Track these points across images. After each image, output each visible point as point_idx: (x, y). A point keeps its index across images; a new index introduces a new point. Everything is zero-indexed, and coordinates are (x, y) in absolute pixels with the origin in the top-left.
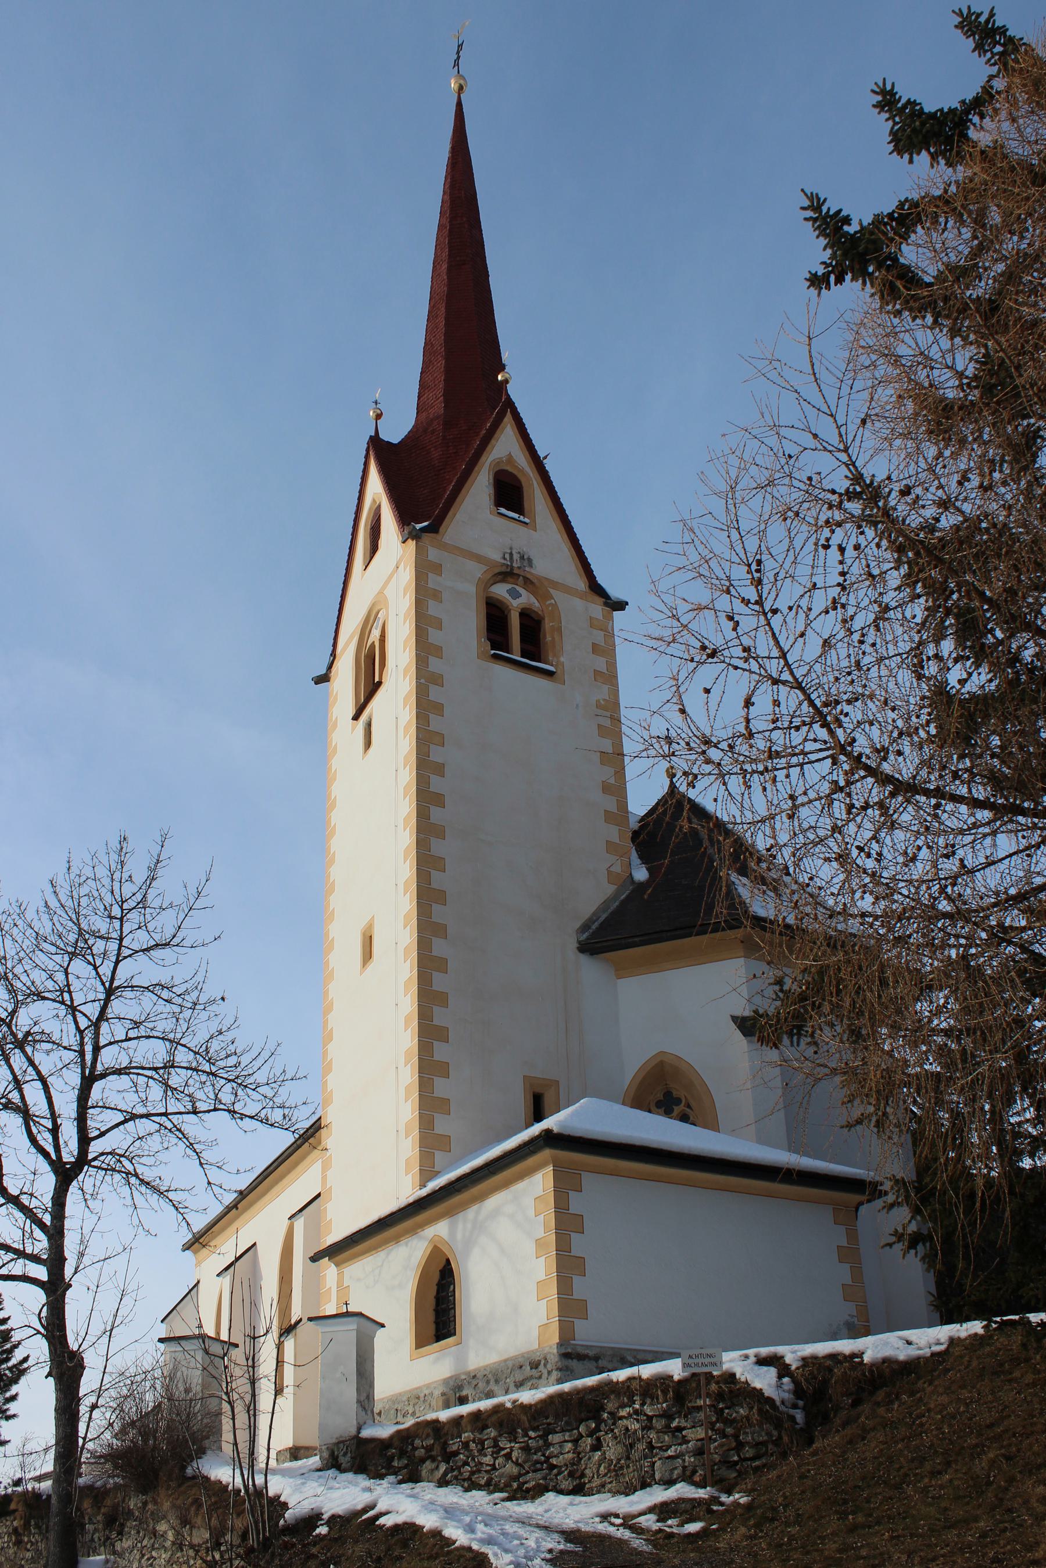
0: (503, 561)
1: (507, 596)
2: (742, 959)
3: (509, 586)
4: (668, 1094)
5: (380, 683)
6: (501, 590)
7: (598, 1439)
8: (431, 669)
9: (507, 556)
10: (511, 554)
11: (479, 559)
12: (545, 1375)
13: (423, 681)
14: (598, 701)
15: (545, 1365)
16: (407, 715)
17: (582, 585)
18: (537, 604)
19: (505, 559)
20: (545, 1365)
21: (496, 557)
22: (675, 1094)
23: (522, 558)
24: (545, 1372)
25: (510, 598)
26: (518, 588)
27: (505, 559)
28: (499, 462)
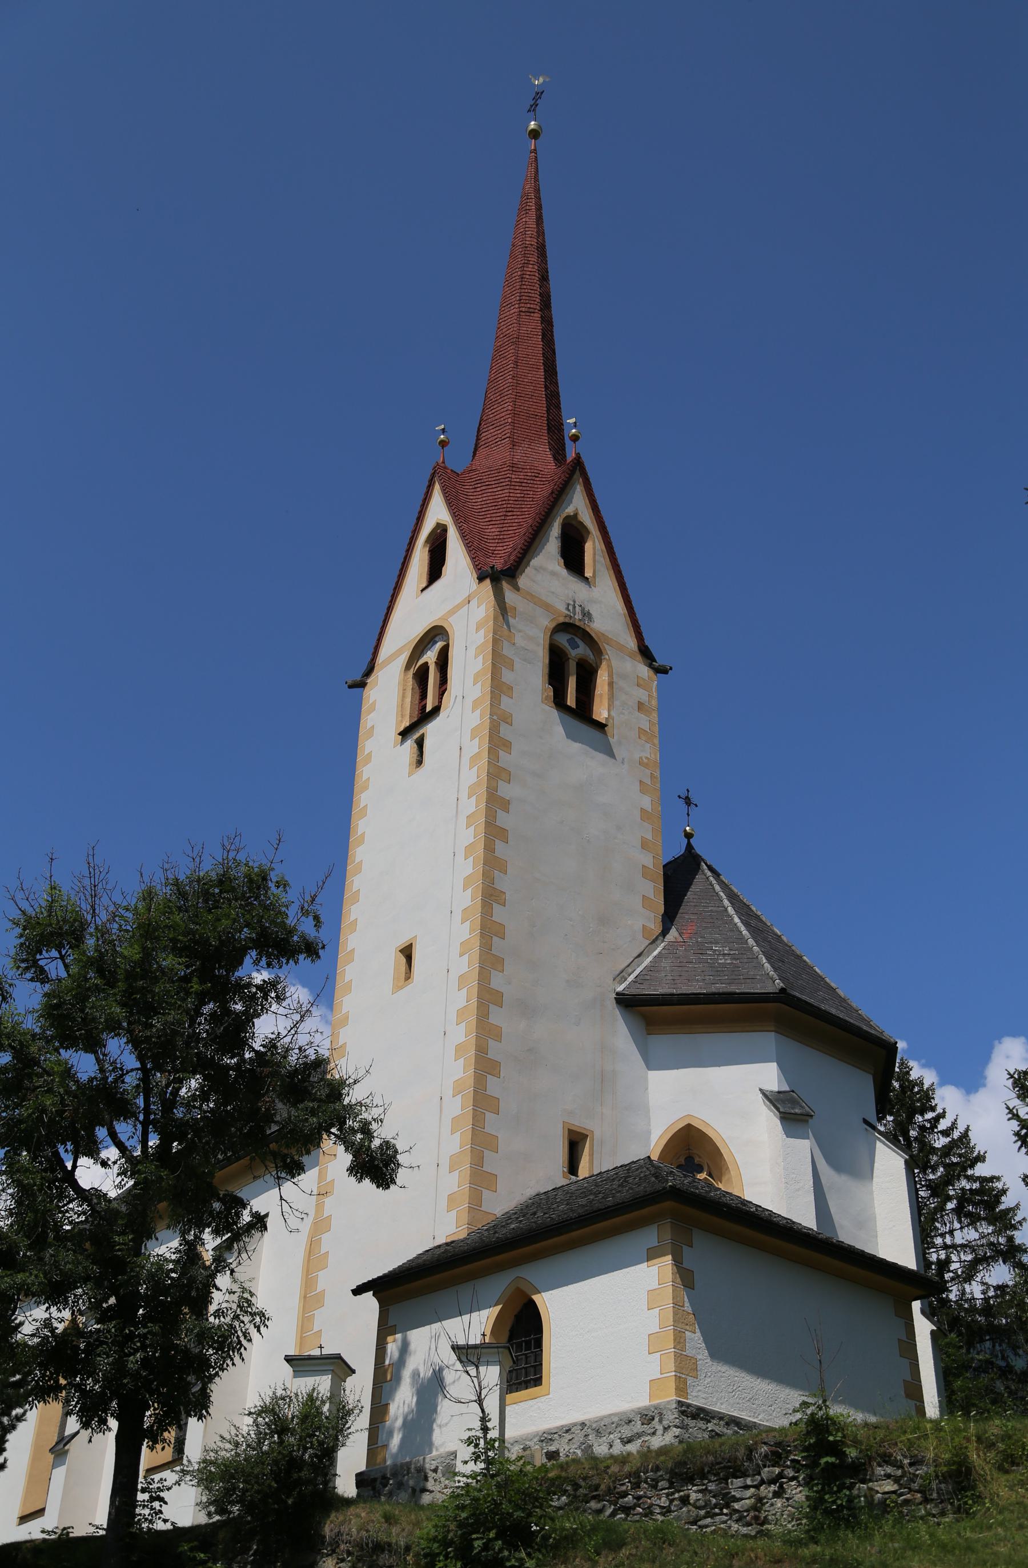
0: (567, 612)
1: (567, 645)
2: (773, 1033)
3: (569, 636)
4: (690, 1159)
5: (436, 710)
6: (563, 640)
7: (781, 1487)
8: (502, 707)
9: (571, 608)
10: (574, 607)
11: (547, 607)
12: (660, 1432)
13: (495, 717)
14: (641, 758)
15: (660, 1421)
16: (476, 746)
17: (632, 643)
18: (592, 657)
19: (569, 610)
20: (660, 1421)
21: (562, 608)
22: (697, 1160)
23: (583, 610)
24: (660, 1428)
25: (569, 648)
26: (577, 640)
27: (569, 610)
28: (568, 517)
